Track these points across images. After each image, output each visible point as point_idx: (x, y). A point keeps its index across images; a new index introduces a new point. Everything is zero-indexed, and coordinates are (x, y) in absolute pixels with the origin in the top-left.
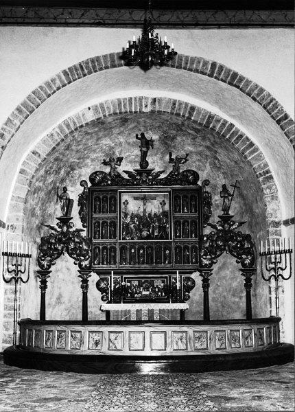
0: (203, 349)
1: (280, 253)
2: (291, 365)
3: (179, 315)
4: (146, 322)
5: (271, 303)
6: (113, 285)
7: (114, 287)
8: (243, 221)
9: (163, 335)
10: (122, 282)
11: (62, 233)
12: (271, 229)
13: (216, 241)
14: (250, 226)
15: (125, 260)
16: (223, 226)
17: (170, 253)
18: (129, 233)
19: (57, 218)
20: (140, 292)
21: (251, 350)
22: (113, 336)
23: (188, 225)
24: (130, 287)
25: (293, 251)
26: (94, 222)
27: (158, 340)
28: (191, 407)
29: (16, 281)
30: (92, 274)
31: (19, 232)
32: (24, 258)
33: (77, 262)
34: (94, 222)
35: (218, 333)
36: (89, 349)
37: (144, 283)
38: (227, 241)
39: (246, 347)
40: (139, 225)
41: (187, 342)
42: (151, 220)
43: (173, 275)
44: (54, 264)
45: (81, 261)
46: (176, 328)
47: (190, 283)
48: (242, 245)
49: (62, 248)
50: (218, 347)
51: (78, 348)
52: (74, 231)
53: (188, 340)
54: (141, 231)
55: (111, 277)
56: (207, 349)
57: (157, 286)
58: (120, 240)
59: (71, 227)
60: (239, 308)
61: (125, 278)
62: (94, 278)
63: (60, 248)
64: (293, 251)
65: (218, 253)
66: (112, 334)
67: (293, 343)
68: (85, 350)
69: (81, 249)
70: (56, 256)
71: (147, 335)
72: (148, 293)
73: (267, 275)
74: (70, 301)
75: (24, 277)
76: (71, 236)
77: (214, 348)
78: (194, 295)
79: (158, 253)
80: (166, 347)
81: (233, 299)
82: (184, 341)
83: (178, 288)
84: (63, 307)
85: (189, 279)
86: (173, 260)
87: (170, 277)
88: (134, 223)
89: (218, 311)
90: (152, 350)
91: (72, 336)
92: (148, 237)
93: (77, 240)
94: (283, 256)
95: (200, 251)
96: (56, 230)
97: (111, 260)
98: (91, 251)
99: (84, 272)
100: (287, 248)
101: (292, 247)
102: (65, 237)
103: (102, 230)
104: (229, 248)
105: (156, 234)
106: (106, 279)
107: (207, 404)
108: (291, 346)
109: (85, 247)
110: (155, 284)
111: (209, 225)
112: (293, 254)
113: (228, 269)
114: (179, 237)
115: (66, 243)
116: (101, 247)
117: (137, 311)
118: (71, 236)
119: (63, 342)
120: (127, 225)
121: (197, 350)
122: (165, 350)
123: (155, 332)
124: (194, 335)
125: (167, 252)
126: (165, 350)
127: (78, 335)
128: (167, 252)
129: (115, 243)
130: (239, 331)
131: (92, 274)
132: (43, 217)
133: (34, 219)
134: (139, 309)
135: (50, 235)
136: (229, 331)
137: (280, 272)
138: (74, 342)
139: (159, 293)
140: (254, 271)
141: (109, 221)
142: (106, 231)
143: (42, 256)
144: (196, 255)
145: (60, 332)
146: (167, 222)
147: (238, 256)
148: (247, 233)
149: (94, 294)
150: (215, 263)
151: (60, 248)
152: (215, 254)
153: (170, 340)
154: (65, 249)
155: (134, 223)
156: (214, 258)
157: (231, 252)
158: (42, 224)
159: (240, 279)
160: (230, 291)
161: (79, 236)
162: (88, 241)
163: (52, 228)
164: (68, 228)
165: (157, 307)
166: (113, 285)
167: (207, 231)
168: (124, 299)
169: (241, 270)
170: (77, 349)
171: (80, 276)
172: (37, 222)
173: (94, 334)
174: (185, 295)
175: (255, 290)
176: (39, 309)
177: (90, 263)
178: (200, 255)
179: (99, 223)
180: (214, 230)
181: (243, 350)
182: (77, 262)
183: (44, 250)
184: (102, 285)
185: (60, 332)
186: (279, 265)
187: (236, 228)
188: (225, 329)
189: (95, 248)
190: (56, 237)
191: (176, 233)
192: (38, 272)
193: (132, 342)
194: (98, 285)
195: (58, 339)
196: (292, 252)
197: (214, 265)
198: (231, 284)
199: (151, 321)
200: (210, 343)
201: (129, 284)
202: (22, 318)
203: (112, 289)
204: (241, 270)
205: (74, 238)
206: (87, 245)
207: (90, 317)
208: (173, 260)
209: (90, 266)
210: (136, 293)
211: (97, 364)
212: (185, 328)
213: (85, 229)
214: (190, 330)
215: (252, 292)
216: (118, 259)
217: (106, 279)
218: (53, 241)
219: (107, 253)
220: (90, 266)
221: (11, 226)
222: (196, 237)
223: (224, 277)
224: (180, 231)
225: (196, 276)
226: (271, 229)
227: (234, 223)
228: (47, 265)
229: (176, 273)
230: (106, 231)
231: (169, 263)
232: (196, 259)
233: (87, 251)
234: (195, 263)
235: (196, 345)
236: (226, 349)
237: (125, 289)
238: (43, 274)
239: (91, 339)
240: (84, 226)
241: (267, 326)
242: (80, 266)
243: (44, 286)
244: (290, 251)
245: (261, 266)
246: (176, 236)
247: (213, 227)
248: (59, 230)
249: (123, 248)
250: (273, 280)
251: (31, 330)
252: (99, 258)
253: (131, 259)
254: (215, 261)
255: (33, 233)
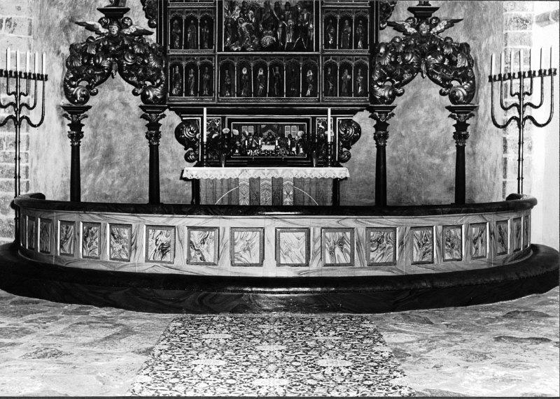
0: (386, 264)
1: (531, 75)
2: (556, 289)
3: (330, 188)
4: (268, 208)
5: (505, 169)
6: (205, 133)
7: (209, 136)
8: (453, 18)
9: (302, 235)
10: (224, 127)
11: (110, 37)
12: (513, 32)
13: (403, 54)
14: (469, 27)
15: (230, 88)
16: (417, 28)
17: (315, 76)
18: (237, 39)
19: (101, 10)
20: (258, 147)
21: (482, 265)
22: (196, 236)
23: (350, 25)
24: (239, 137)
25: (558, 72)
26: (170, 17)
27: (294, 244)
28: (348, 354)
29: (18, 124)
30: (167, 112)
31: (22, 32)
32: (33, 82)
33: (140, 91)
34: (170, 17)
35: (418, 232)
36: (147, 260)
37: (265, 130)
38: (424, 55)
39: (473, 258)
40: (256, 25)
41: (352, 249)
42: (279, 16)
43: (320, 117)
44: (95, 94)
45: (147, 88)
46: (331, 221)
47: (351, 131)
48: (453, 63)
49: (111, 65)
50: (416, 259)
51: (124, 257)
52: (133, 35)
53: (356, 244)
54: (260, 35)
55: (202, 118)
56: (394, 263)
57: (290, 136)
58: (220, 50)
59: (127, 27)
60: (440, 175)
61: (230, 121)
62: (171, 119)
63: (106, 64)
64: (558, 72)
65: (407, 77)
66: (196, 233)
67: (558, 250)
68: (141, 263)
69: (146, 66)
70: (98, 79)
71: (270, 234)
72: (272, 148)
73: (501, 117)
74: (128, 160)
75: (35, 117)
76: (126, 42)
77: (409, 262)
78: (358, 152)
79: (293, 76)
80: (308, 258)
81: (430, 160)
82: (347, 247)
83: (329, 140)
84: (116, 170)
85: (350, 122)
86: (321, 88)
87: (314, 119)
88: (247, 19)
89: (400, 180)
90: (279, 265)
91: (112, 234)
92: (274, 47)
93: (137, 50)
94: (537, 80)
95: (372, 72)
96: (97, 32)
97: (204, 87)
98: (165, 70)
99: (152, 111)
100: (546, 67)
101: (555, 65)
102: (115, 45)
103: (186, 33)
104: (427, 68)
105: (289, 40)
106: (193, 122)
107: (364, 326)
108: (551, 255)
109: (154, 64)
110: (287, 133)
111: (390, 24)
112: (556, 78)
113: (422, 106)
114: (334, 46)
115: (118, 56)
116: (184, 64)
117: (252, 180)
118: (126, 42)
119: (94, 244)
120: (235, 24)
121: (373, 265)
122: (307, 265)
123: (285, 229)
124: (368, 236)
125: (310, 74)
126: (307, 265)
127: (125, 233)
128: (310, 74)
129: (210, 57)
130: (460, 227)
131: (167, 112)
132: (74, 8)
133: (54, 10)
134: (256, 176)
135: (87, 40)
136: (440, 228)
137: (528, 111)
138: (118, 247)
139: (294, 149)
140: (471, 111)
141: (199, 17)
142: (194, 35)
143: (73, 79)
144: (365, 79)
145: (89, 225)
146: (310, 19)
147: (445, 83)
148: (462, 40)
149: (171, 149)
150: (400, 95)
151: (106, 64)
152: (400, 78)
153: (318, 245)
154: (115, 66)
155: (247, 19)
156: (397, 86)
157: (430, 75)
158: (72, 20)
159: (448, 124)
160: (424, 145)
161: (142, 44)
162: (161, 53)
163: (90, 28)
164: (120, 28)
165: (288, 173)
166: (205, 133)
167: (386, 36)
168: (228, 158)
169: (449, 108)
170: (124, 260)
171: (143, 117)
172: (62, 16)
173: (159, 231)
174: (341, 153)
175: (473, 144)
176: (70, 174)
177: (164, 92)
178: (371, 79)
179: (180, 19)
180: (401, 35)
181: (467, 264)
182: (140, 91)
183: (76, 68)
184: (187, 133)
185: (89, 225)
186: (527, 99)
187: (442, 31)
188: (459, 222)
189: (173, 66)
190: (98, 46)
191: (327, 39)
192: (65, 108)
193: (237, 249)
194: (178, 133)
195: (85, 239)
196: (555, 73)
197: (397, 98)
198: (426, 134)
199: (277, 206)
200: (402, 250)
201: (236, 132)
202: (32, 191)
203: (205, 140)
204: (449, 108)
205: (132, 46)
206: (157, 58)
207: (164, 198)
208: (321, 88)
209: (164, 99)
210: (250, 147)
211: (162, 292)
212: (349, 222)
213: (154, 30)
214: (359, 225)
215: (468, 149)
216: (216, 85)
217: (193, 122)
218: (93, 52)
219: (195, 74)
220: (164, 99)
221: (8, 20)
222: (365, 46)
223: (414, 122)
224: (334, 35)
225: (364, 120)
226: (513, 32)
227: (438, 20)
228: (82, 96)
229: (325, 112)
230: (194, 35)
231: (314, 94)
232: (364, 88)
233: (158, 70)
234: (362, 94)
235: (372, 255)
236: (433, 262)
237: (230, 139)
238: (75, 112)
239: (152, 242)
240: (150, 25)
241: (514, 216)
242: (144, 97)
243: (76, 133)
244: (552, 73)
245: (486, 99)
246: (327, 45)
247: (399, 28)
248: (103, 30)
249: (226, 67)
250: (513, 127)
251: (33, 219)
252: (182, 85)
253: (241, 86)
254: (400, 91)
255: (52, 36)
